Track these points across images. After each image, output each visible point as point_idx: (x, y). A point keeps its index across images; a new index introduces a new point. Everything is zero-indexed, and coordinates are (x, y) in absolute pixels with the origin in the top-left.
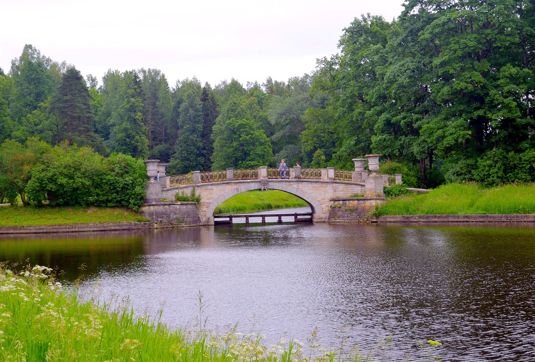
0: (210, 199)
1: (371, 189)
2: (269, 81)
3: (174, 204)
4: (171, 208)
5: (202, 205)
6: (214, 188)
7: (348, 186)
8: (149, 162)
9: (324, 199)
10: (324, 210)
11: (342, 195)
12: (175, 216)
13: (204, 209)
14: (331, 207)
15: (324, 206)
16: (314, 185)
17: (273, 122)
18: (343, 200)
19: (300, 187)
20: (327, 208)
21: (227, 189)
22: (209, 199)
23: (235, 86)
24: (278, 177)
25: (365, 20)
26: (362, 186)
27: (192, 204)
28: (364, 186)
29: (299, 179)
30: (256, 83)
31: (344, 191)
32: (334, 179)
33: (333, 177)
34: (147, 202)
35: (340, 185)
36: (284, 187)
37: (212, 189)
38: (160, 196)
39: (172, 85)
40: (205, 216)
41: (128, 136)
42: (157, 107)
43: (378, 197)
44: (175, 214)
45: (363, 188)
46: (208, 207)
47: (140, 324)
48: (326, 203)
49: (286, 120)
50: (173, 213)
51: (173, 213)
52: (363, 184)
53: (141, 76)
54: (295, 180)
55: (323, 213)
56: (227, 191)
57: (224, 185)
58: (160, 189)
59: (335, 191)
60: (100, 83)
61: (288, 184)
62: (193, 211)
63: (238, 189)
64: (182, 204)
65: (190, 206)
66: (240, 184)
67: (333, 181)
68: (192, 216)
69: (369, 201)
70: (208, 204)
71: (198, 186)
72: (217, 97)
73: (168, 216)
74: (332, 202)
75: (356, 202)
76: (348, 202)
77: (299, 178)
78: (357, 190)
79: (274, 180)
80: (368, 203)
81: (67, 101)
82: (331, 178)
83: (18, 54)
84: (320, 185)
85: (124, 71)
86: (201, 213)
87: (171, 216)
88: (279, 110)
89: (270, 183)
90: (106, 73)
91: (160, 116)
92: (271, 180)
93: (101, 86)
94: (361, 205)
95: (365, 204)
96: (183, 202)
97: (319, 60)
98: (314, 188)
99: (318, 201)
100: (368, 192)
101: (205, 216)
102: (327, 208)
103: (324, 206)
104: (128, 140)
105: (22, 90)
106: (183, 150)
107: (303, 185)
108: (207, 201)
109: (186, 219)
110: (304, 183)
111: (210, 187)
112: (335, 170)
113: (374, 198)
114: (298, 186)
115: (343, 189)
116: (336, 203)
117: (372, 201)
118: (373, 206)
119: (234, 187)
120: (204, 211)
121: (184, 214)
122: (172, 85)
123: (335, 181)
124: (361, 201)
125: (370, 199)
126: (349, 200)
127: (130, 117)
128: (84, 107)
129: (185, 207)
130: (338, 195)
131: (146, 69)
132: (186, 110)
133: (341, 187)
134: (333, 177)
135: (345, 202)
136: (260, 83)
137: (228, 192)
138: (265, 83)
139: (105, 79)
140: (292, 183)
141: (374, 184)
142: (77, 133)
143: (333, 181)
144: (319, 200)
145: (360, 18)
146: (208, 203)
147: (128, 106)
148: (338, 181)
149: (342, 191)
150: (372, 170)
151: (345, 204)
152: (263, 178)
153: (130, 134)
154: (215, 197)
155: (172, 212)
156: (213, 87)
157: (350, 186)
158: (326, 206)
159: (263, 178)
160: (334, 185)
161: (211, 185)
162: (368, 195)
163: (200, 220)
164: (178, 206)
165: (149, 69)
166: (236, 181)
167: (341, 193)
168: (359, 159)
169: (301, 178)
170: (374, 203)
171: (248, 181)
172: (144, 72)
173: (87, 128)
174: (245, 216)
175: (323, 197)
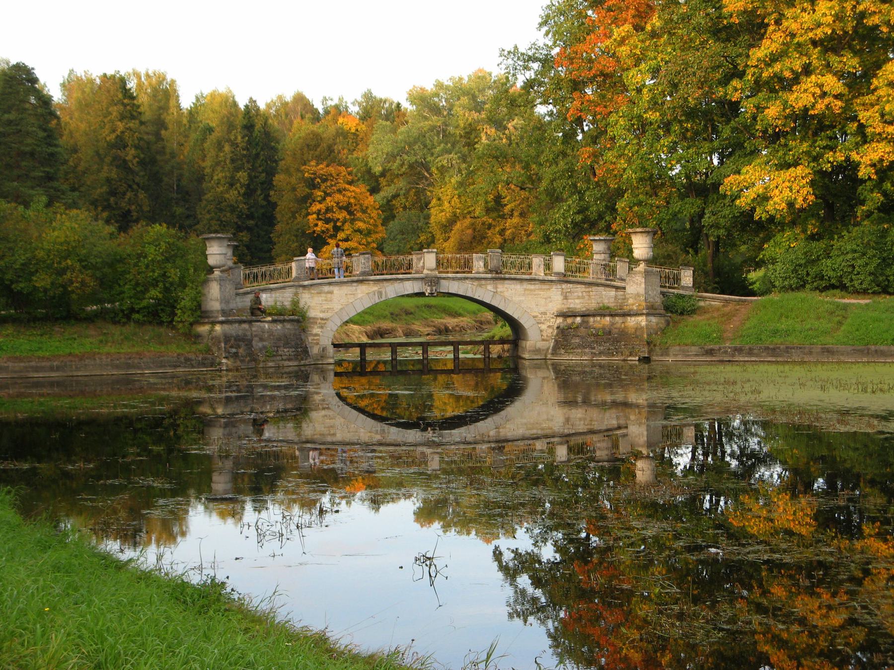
0: (328, 310)
1: (638, 295)
2: (368, 96)
3: (259, 321)
4: (254, 329)
5: (312, 323)
6: (336, 290)
8: (212, 238)
9: (545, 313)
10: (545, 334)
11: (578, 306)
12: (260, 345)
13: (316, 330)
14: (558, 328)
15: (544, 327)
16: (526, 285)
17: (377, 169)
18: (582, 316)
20: (550, 330)
21: (359, 291)
23: (302, 104)
24: (449, 270)
25: (83, 92)
26: (617, 288)
27: (292, 321)
28: (624, 288)
29: (498, 274)
30: (341, 99)
31: (583, 297)
32: (565, 276)
33: (563, 271)
34: (208, 317)
35: (575, 286)
36: (470, 290)
37: (331, 293)
38: (232, 305)
39: (186, 102)
40: (318, 344)
41: (113, 193)
42: (163, 140)
43: (651, 311)
44: (261, 340)
45: (620, 293)
46: (322, 327)
48: (549, 321)
49: (402, 165)
50: (257, 339)
51: (257, 339)
53: (132, 85)
54: (489, 276)
55: (543, 340)
56: (360, 296)
57: (355, 284)
59: (566, 298)
61: (476, 283)
62: (294, 334)
63: (380, 293)
64: (274, 321)
65: (288, 326)
66: (385, 284)
67: (564, 279)
68: (293, 343)
69: (633, 319)
70: (323, 322)
71: (304, 287)
72: (274, 123)
73: (249, 343)
74: (560, 320)
75: (237, 325)
76: (591, 319)
77: (497, 273)
78: (608, 297)
79: (450, 275)
80: (632, 322)
81: (10, 123)
82: (558, 274)
84: (537, 286)
85: (101, 73)
86: (310, 338)
87: (254, 343)
88: (387, 148)
89: (443, 282)
90: (66, 77)
91: (168, 157)
92: (444, 275)
94: (618, 325)
95: (627, 324)
96: (276, 318)
98: (527, 292)
99: (534, 317)
100: (631, 301)
101: (318, 344)
102: (550, 330)
103: (544, 327)
104: (112, 199)
106: (212, 219)
107: (506, 286)
108: (321, 315)
109: (282, 349)
110: (507, 282)
111: (326, 288)
112: (565, 256)
113: (644, 311)
114: (496, 288)
115: (580, 294)
116: (569, 320)
117: (640, 318)
118: (642, 328)
119: (375, 288)
120: (316, 335)
121: (279, 339)
122: (186, 102)
123: (565, 279)
126: (594, 316)
127: (115, 158)
128: (42, 134)
129: (279, 327)
130: (572, 306)
132: (219, 146)
134: (563, 271)
135: (586, 319)
137: (361, 298)
138: (360, 99)
140: (483, 282)
141: (643, 286)
142: (29, 183)
143: (562, 278)
144: (535, 314)
146: (322, 319)
147: (113, 136)
148: (571, 279)
149: (578, 298)
150: (640, 258)
151: (588, 322)
152: (429, 272)
153: (115, 189)
154: (337, 307)
155: (256, 336)
156: (262, 106)
157: (594, 288)
158: (549, 327)
159: (429, 272)
160: (564, 286)
161: (330, 284)
162: (633, 304)
163: (307, 352)
164: (267, 326)
166: (378, 277)
167: (577, 301)
168: (602, 238)
169: (501, 273)
170: (642, 321)
171: (400, 276)
172: (137, 75)
173: (48, 173)
174: (391, 345)
175: (542, 309)
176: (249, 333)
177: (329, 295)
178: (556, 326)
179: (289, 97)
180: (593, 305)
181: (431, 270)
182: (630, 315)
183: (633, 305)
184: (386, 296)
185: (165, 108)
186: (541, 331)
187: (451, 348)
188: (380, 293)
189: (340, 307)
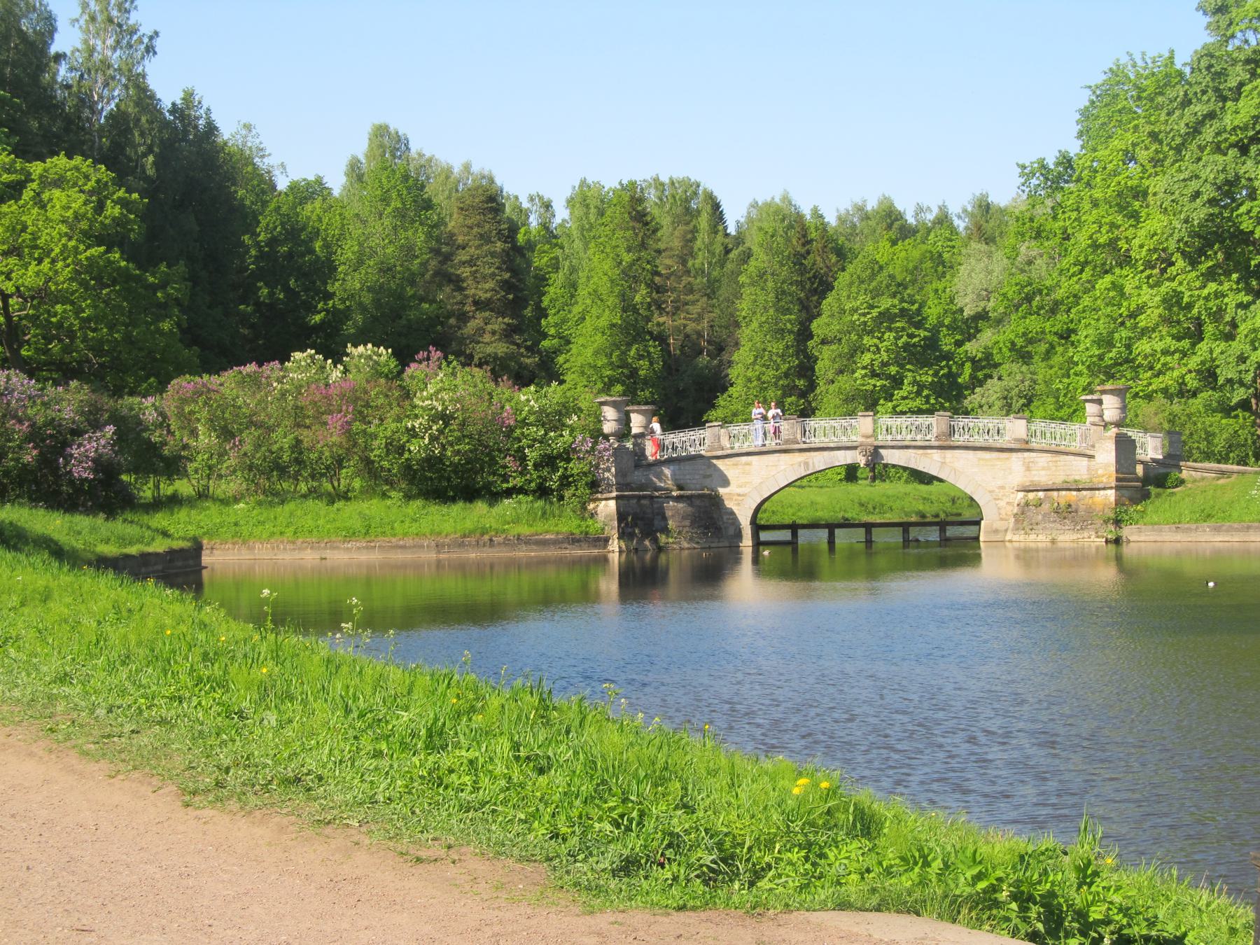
2: (583, 183)
7: (1057, 459)
9: (1002, 487)
10: (1003, 512)
15: (1002, 503)
19: (947, 460)
20: (1009, 508)
22: (741, 487)
31: (1048, 469)
36: (913, 460)
45: (1093, 462)
46: (739, 504)
47: (145, 578)
52: (1091, 453)
56: (783, 467)
58: (631, 464)
59: (1028, 469)
60: (561, 214)
63: (806, 464)
69: (1102, 492)
70: (741, 498)
74: (1021, 495)
75: (1074, 493)
83: (360, 147)
86: (725, 517)
93: (564, 220)
94: (1086, 501)
97: (1024, 167)
98: (982, 462)
99: (990, 492)
103: (1002, 503)
105: (1158, 81)
108: (739, 491)
124: (1084, 493)
125: (1104, 489)
126: (1058, 490)
130: (1036, 479)
131: (665, 179)
133: (1043, 459)
134: (1024, 437)
136: (954, 209)
139: (570, 202)
143: (1024, 446)
144: (991, 489)
145: (1124, 60)
146: (739, 495)
149: (1043, 469)
152: (864, 440)
156: (831, 219)
159: (864, 440)
160: (1026, 454)
165: (671, 179)
167: (1043, 473)
175: (1000, 483)
176: (649, 511)
177: (747, 467)
178: (1016, 502)
179: (312, 178)
180: (1059, 479)
181: (868, 437)
182: (1098, 489)
183: (1103, 476)
184: (814, 466)
185: (825, 230)
186: (999, 509)
187: (862, 530)
188: (806, 464)
189: (759, 481)
